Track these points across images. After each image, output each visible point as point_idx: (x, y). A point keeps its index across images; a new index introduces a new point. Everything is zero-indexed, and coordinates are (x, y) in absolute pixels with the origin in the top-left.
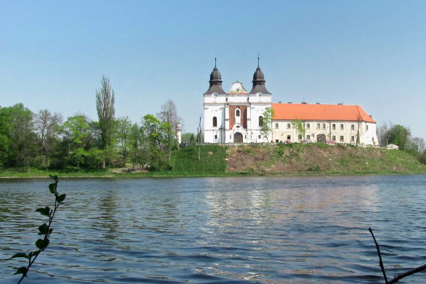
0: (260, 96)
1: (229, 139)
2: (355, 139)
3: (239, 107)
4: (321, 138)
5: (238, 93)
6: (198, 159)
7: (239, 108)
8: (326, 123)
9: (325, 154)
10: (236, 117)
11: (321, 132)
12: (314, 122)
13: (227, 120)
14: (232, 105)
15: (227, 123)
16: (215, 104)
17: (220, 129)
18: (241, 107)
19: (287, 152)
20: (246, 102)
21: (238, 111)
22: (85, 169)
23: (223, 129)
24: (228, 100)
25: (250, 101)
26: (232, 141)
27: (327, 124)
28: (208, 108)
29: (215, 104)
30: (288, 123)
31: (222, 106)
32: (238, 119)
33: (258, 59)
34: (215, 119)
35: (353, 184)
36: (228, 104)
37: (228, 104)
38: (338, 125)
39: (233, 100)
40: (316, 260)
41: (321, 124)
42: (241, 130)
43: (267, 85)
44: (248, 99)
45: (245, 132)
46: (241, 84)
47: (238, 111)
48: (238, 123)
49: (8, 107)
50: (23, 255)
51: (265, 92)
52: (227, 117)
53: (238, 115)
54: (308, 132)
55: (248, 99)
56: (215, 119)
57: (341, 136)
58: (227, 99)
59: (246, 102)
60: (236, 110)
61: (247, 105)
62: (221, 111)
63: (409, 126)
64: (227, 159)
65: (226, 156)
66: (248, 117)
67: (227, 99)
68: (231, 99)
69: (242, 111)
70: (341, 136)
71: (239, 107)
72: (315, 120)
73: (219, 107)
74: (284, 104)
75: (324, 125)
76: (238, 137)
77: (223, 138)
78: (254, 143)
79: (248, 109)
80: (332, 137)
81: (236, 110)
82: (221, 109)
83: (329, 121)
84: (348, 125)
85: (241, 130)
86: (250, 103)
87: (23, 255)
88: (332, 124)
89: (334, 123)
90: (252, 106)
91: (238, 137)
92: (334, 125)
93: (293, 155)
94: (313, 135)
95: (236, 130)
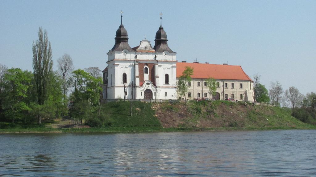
0: (166, 54)
1: (140, 96)
2: (244, 96)
3: (147, 64)
5: (145, 51)
6: (130, 115)
7: (147, 66)
8: (220, 82)
9: (234, 111)
10: (144, 74)
12: (237, 82)
13: (138, 77)
14: (141, 62)
15: (138, 80)
16: (125, 61)
17: (129, 85)
18: (149, 65)
19: (203, 109)
20: (153, 60)
21: (146, 69)
23: (133, 86)
24: (137, 58)
25: (157, 59)
26: (142, 97)
27: (221, 84)
29: (125, 61)
30: (198, 81)
31: (131, 64)
32: (146, 77)
34: (125, 76)
36: (137, 61)
38: (229, 84)
39: (142, 57)
40: (293, 174)
42: (151, 87)
43: (170, 44)
44: (156, 57)
45: (154, 88)
47: (146, 69)
48: (148, 81)
50: (286, 135)
51: (170, 52)
52: (137, 74)
53: (146, 72)
54: (190, 89)
55: (156, 57)
56: (125, 76)
57: (165, 93)
58: (136, 56)
60: (145, 67)
61: (155, 63)
62: (131, 68)
63: (209, 76)
64: (156, 115)
65: (154, 112)
66: (156, 74)
67: (136, 56)
68: (141, 57)
69: (150, 69)
70: (165, 93)
71: (147, 64)
73: (129, 64)
74: (179, 63)
76: (148, 93)
77: (133, 94)
78: (172, 100)
79: (156, 66)
81: (145, 67)
82: (130, 66)
83: (222, 80)
84: (237, 84)
85: (151, 87)
86: (158, 61)
87: (286, 135)
88: (225, 82)
90: (159, 64)
91: (148, 93)
92: (226, 84)
93: (209, 112)
95: (146, 87)
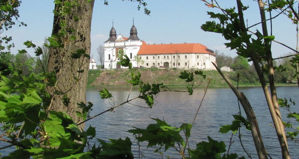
4: (166, 64)
11: (154, 61)
16: (109, 47)
20: (124, 45)
22: (35, 89)
25: (125, 45)
27: (170, 56)
28: (106, 50)
29: (109, 47)
33: (133, 20)
35: (96, 87)
37: (115, 47)
41: (166, 56)
43: (139, 35)
44: (115, 44)
46: (122, 35)
49: (169, 43)
59: (124, 45)
72: (163, 54)
73: (111, 49)
75: (168, 56)
79: (124, 49)
80: (173, 64)
83: (171, 54)
89: (174, 55)
90: (126, 48)
94: (161, 62)
